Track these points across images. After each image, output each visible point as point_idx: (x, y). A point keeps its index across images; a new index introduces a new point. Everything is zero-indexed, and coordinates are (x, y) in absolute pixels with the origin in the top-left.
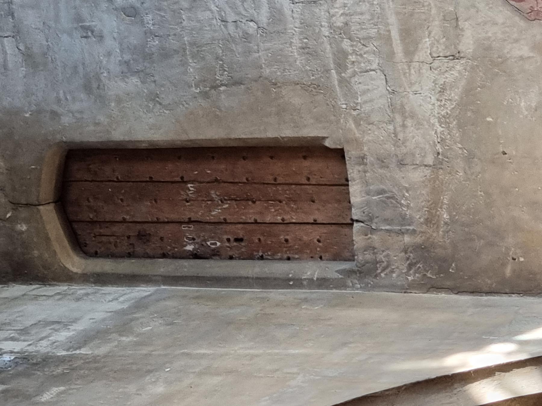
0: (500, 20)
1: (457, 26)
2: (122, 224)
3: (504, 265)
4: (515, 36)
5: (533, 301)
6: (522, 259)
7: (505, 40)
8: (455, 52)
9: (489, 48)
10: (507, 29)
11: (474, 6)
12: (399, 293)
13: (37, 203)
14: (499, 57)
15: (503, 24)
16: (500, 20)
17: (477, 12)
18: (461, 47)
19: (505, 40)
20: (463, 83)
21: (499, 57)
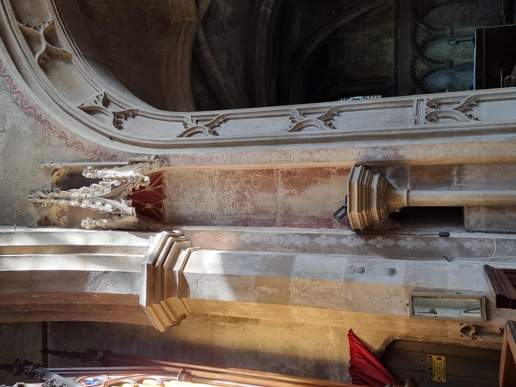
0: (19, 116)
1: (5, 119)
2: (182, 132)
3: (13, 214)
4: (24, 123)
5: (220, 229)
6: (19, 211)
7: (20, 124)
8: (4, 129)
9: (15, 128)
10: (21, 120)
11: (11, 111)
12: (131, 246)
13: (59, 224)
14: (18, 131)
15: (20, 118)
16: (19, 116)
17: (12, 113)
18: (6, 128)
19: (20, 124)
20: (6, 141)
21: (18, 131)
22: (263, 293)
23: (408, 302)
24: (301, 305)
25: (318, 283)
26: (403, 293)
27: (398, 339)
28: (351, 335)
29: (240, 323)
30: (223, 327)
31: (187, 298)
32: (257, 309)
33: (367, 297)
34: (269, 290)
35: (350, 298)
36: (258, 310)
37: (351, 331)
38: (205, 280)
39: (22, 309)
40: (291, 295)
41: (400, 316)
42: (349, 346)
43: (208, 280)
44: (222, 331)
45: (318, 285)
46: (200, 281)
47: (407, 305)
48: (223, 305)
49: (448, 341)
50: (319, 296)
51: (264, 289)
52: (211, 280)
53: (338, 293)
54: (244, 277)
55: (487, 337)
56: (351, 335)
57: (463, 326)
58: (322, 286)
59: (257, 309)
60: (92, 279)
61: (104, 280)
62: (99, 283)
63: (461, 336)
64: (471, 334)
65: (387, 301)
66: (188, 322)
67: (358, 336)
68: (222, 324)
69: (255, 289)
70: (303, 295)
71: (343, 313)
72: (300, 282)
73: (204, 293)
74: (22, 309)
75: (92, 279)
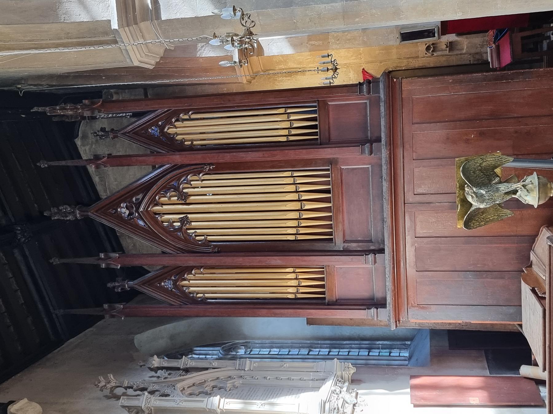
22: (312, 45)
23: (398, 36)
24: (337, 49)
25: (346, 33)
26: (395, 32)
27: (391, 70)
28: (364, 71)
29: (293, 76)
30: (281, 81)
31: (262, 56)
32: (308, 57)
33: (375, 37)
34: (316, 43)
35: (365, 40)
36: (309, 58)
37: (363, 69)
38: (274, 43)
39: (150, 73)
40: (330, 43)
41: (393, 45)
42: (362, 78)
43: (276, 43)
44: (281, 84)
45: (347, 35)
46: (270, 44)
47: (397, 38)
48: (285, 58)
49: (419, 65)
50: (348, 42)
51: (313, 42)
52: (278, 42)
53: (358, 38)
54: (300, 37)
55: (439, 52)
56: (364, 71)
57: (427, 46)
58: (349, 35)
59: (308, 57)
60: (199, 48)
61: (207, 48)
62: (204, 50)
63: (426, 54)
64: (431, 52)
65: (386, 38)
66: (257, 82)
67: (368, 71)
68: (280, 79)
69: (307, 43)
70: (338, 42)
71: (362, 49)
72: (335, 35)
73: (274, 51)
74: (150, 73)
75: (199, 48)
